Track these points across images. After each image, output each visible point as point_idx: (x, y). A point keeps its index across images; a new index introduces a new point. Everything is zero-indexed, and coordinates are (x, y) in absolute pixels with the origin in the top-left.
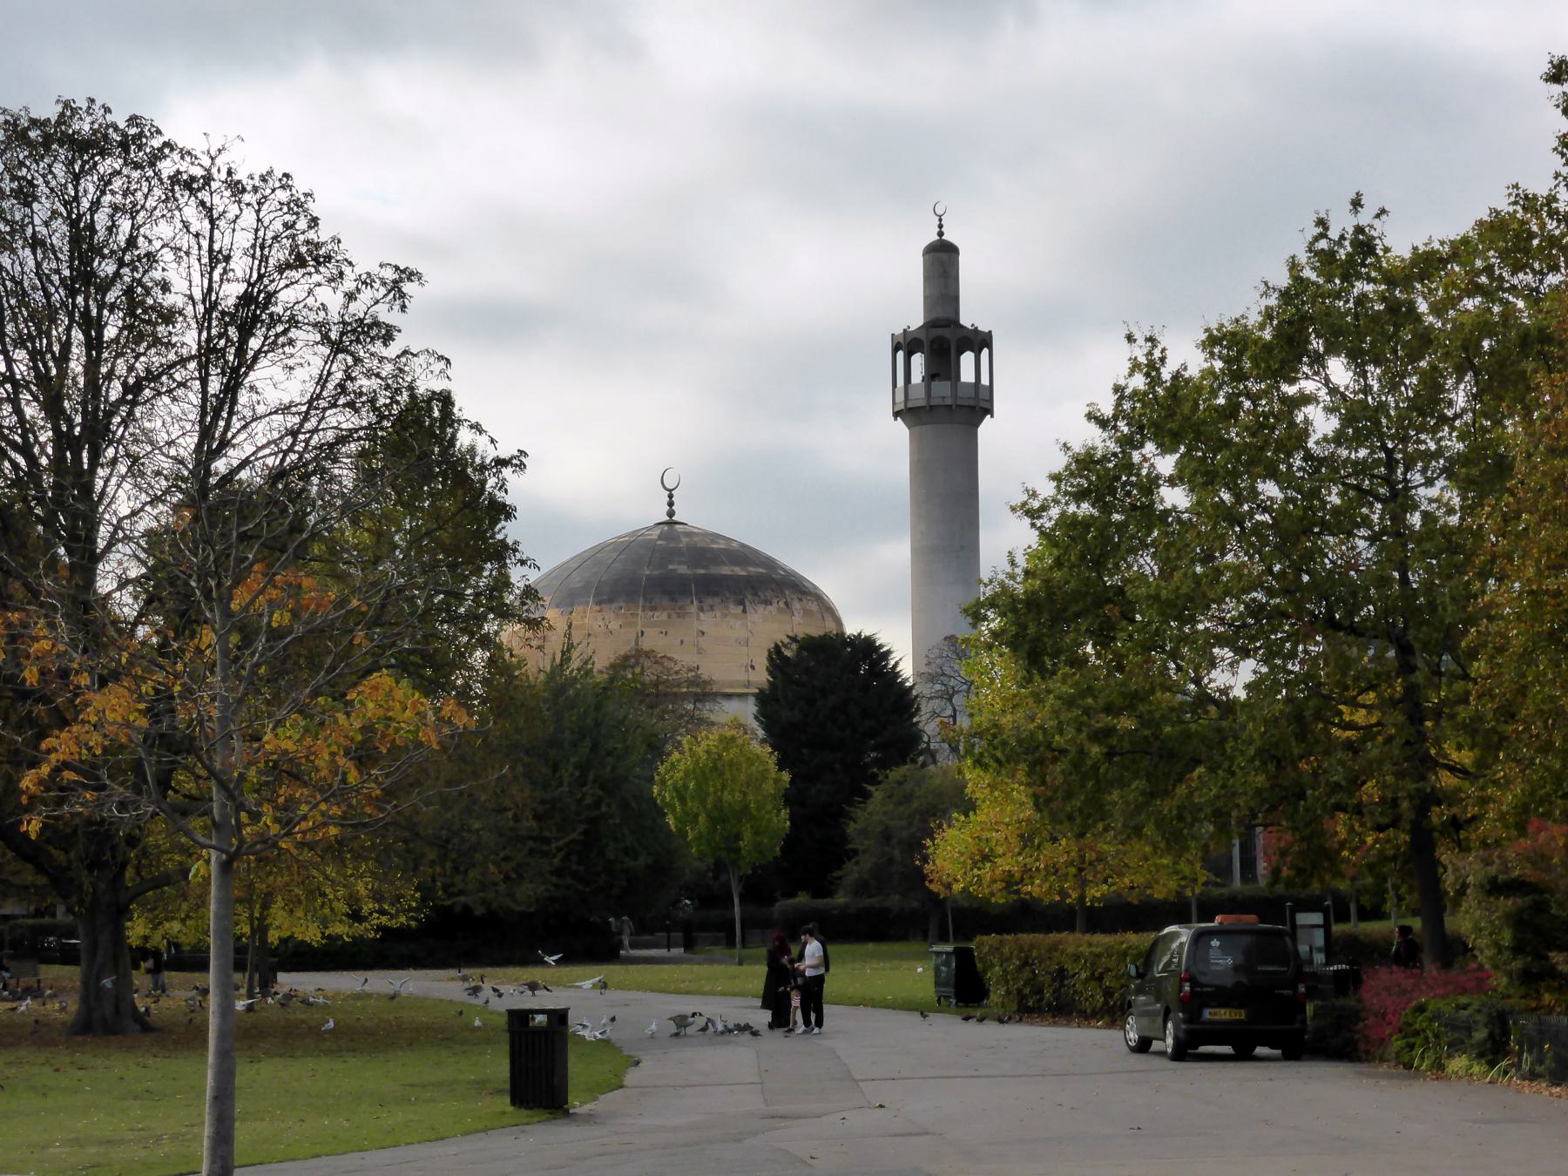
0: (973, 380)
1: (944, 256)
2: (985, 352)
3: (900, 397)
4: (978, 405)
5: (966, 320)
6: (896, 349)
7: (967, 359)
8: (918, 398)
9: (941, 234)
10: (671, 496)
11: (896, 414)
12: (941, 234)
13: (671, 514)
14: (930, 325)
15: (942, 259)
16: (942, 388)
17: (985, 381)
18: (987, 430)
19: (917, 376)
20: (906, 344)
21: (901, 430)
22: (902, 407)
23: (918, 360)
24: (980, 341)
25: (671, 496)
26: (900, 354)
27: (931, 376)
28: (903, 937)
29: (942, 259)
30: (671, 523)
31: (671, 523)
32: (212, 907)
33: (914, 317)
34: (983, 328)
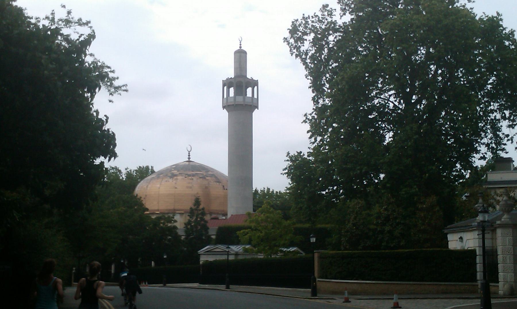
0: (251, 96)
1: (243, 55)
2: (256, 87)
3: (225, 101)
5: (249, 76)
7: (249, 90)
8: (231, 102)
9: (240, 47)
10: (189, 153)
11: (224, 107)
12: (240, 47)
15: (241, 56)
16: (240, 99)
17: (255, 97)
18: (256, 114)
19: (232, 94)
20: (228, 84)
21: (225, 113)
22: (225, 105)
23: (232, 90)
24: (254, 84)
25: (189, 153)
26: (225, 88)
27: (236, 94)
28: (509, 181)
29: (241, 56)
30: (189, 161)
31: (189, 161)
32: (331, 252)
33: (231, 74)
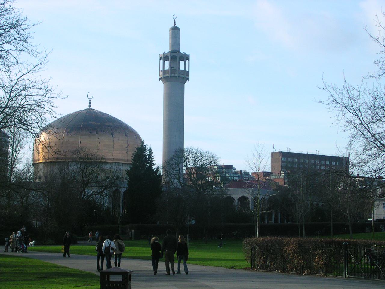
4: (185, 76)
6: (161, 59)
9: (175, 25)
11: (160, 79)
13: (90, 106)
14: (172, 52)
20: (164, 58)
24: (186, 58)
34: (187, 53)
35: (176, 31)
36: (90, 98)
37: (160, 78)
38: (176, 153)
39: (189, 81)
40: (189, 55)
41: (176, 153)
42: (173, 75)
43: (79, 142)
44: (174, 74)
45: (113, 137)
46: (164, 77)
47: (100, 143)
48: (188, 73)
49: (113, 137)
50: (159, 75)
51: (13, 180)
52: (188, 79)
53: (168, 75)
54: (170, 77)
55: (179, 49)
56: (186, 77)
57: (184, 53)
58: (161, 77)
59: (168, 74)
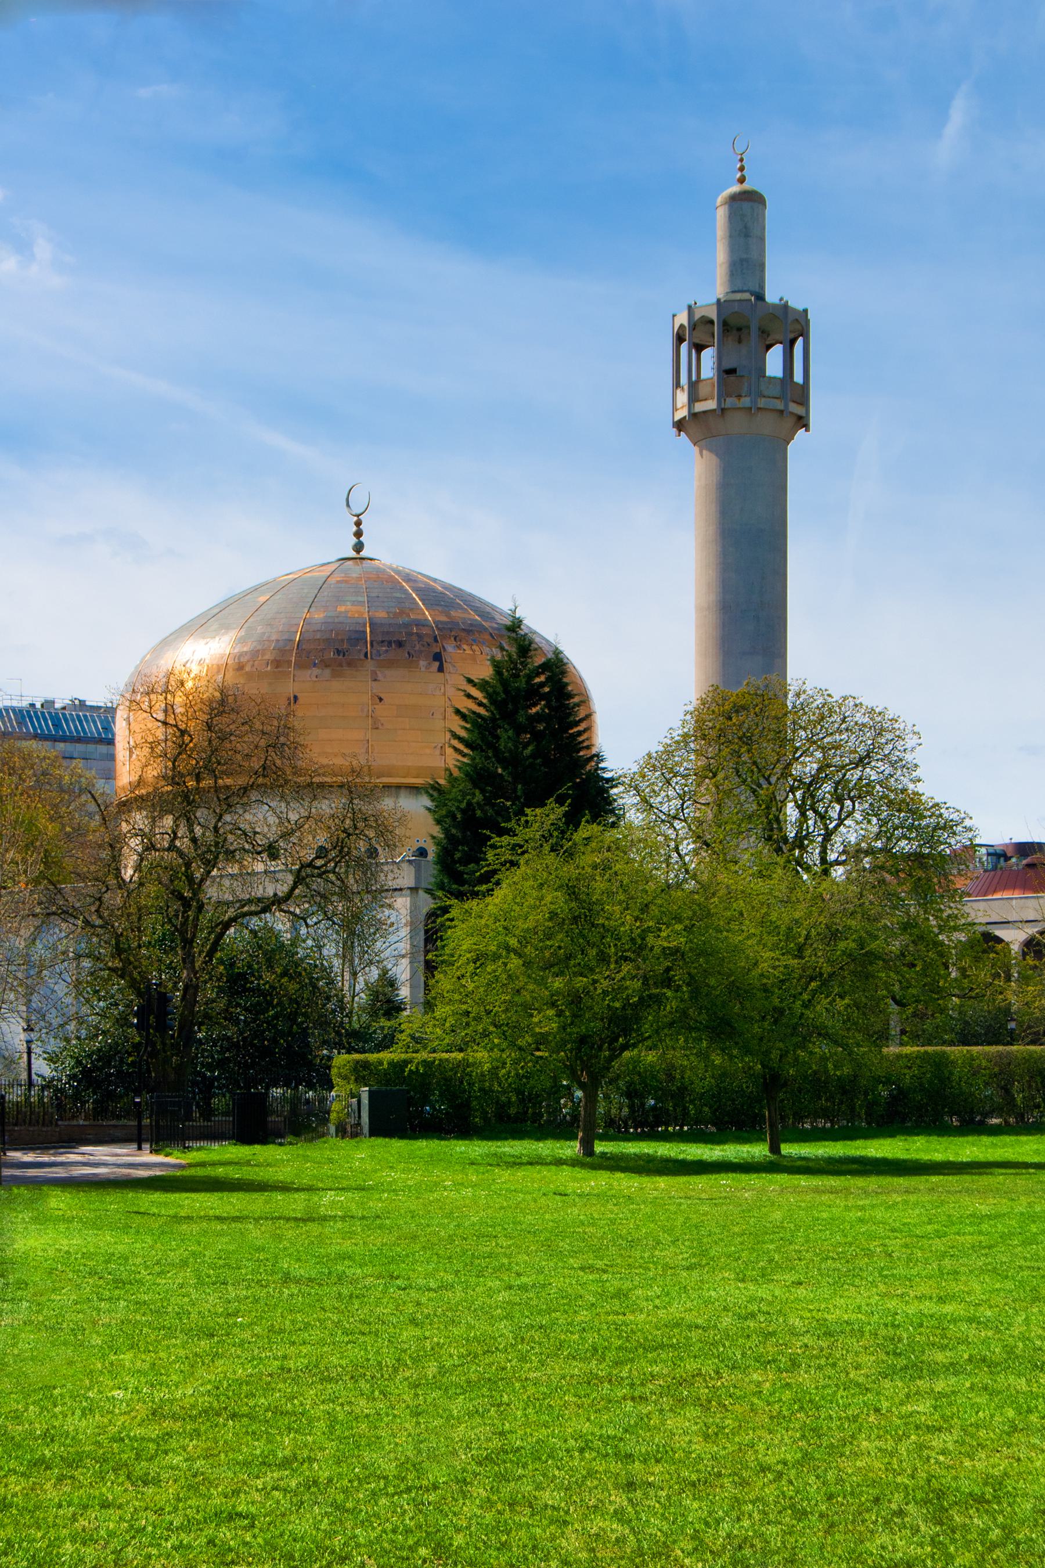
4: (792, 406)
6: (680, 339)
20: (693, 335)
35: (746, 206)
36: (359, 512)
37: (677, 418)
38: (750, 725)
39: (807, 430)
40: (806, 311)
41: (750, 725)
42: (730, 402)
43: (289, 699)
44: (739, 396)
45: (441, 669)
46: (694, 416)
47: (381, 699)
48: (801, 395)
49: (441, 669)
50: (675, 409)
51: (767, 961)
52: (802, 422)
53: (711, 405)
54: (719, 412)
55: (762, 287)
56: (794, 408)
57: (781, 299)
58: (682, 413)
59: (713, 398)
